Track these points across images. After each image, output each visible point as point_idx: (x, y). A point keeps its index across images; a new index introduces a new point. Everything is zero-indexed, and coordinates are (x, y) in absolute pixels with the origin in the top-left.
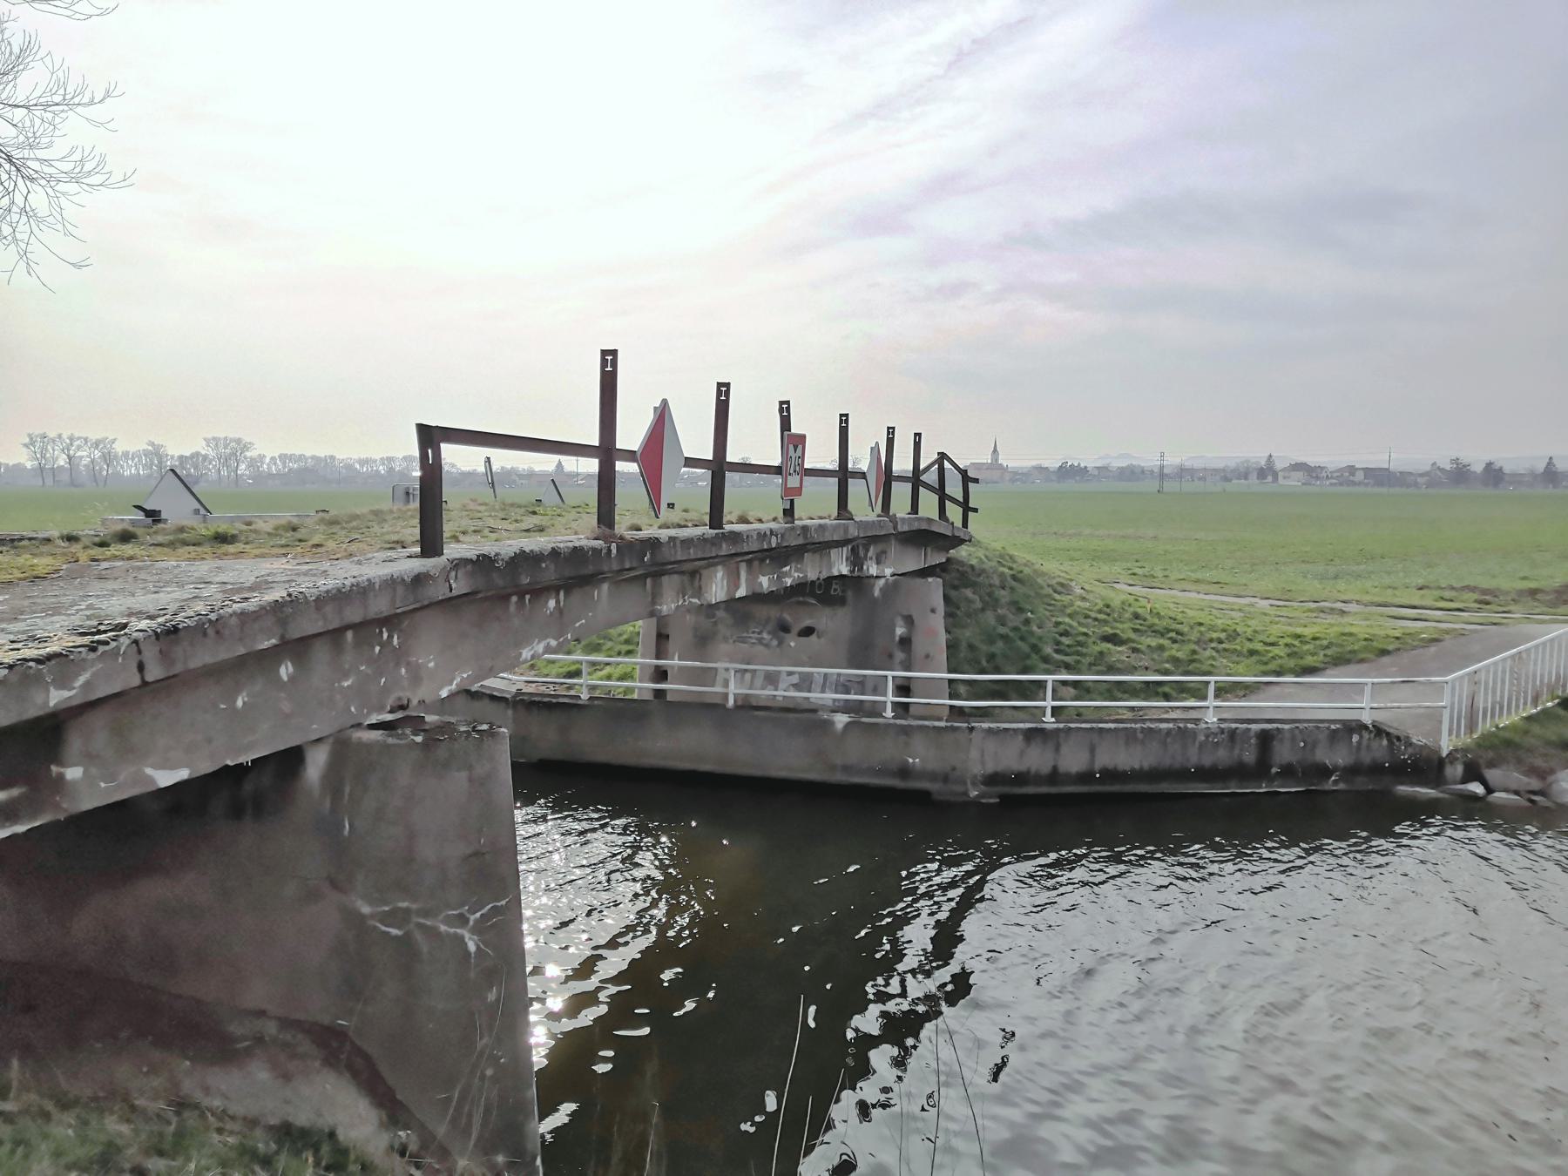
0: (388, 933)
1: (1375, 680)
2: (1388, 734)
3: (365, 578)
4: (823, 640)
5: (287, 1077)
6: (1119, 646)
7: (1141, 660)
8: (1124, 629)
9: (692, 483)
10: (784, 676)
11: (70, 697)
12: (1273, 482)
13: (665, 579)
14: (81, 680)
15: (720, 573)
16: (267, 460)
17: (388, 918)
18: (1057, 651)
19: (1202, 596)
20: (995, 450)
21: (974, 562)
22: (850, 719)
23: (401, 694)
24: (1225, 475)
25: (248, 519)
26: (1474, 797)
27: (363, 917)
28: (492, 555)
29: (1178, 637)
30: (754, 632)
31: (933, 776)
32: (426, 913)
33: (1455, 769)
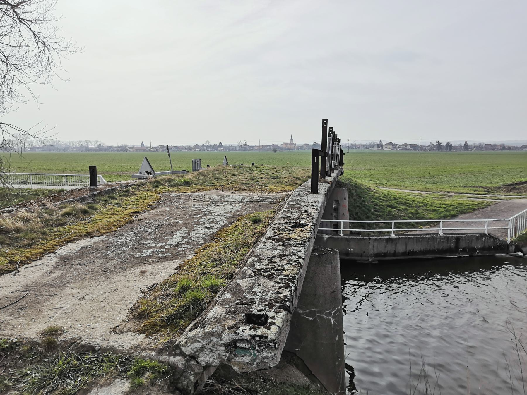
0: (309, 319)
1: (489, 220)
2: (493, 237)
6: (394, 209)
7: (402, 213)
8: (393, 203)
9: (189, 150)
12: (382, 149)
18: (376, 211)
19: (402, 191)
20: (292, 138)
21: (343, 181)
22: (328, 237)
24: (367, 147)
26: (520, 257)
27: (300, 314)
29: (410, 206)
31: (357, 255)
32: (320, 312)
33: (513, 248)
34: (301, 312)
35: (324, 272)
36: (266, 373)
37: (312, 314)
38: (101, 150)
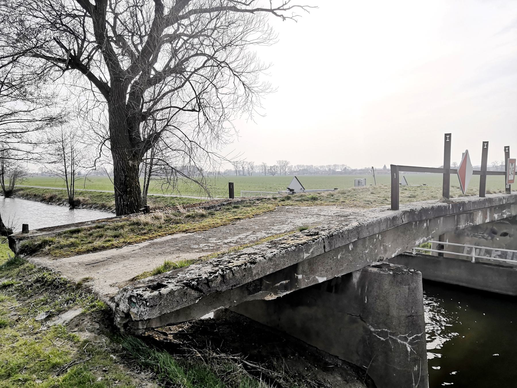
0: (380, 339)
3: (379, 218)
4: (512, 238)
5: (347, 381)
10: (493, 252)
11: (308, 256)
13: (461, 216)
14: (311, 250)
15: (480, 213)
16: (293, 167)
17: (380, 334)
23: (381, 256)
25: (319, 192)
27: (371, 332)
28: (414, 209)
30: (480, 233)
32: (393, 334)
34: (372, 329)
35: (399, 293)
36: (328, 380)
37: (385, 334)
38: (345, 173)
